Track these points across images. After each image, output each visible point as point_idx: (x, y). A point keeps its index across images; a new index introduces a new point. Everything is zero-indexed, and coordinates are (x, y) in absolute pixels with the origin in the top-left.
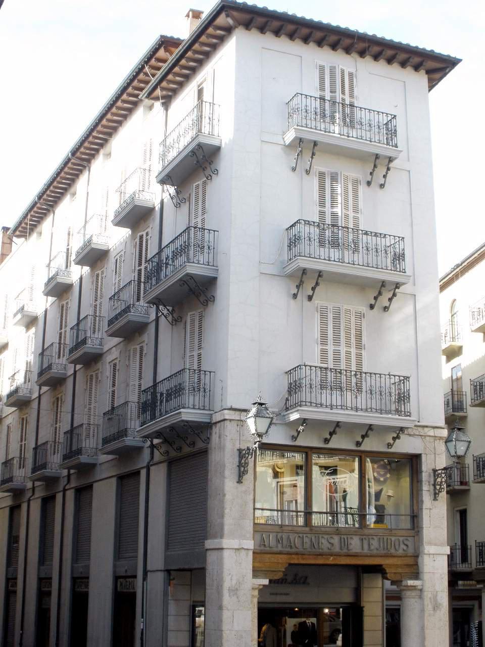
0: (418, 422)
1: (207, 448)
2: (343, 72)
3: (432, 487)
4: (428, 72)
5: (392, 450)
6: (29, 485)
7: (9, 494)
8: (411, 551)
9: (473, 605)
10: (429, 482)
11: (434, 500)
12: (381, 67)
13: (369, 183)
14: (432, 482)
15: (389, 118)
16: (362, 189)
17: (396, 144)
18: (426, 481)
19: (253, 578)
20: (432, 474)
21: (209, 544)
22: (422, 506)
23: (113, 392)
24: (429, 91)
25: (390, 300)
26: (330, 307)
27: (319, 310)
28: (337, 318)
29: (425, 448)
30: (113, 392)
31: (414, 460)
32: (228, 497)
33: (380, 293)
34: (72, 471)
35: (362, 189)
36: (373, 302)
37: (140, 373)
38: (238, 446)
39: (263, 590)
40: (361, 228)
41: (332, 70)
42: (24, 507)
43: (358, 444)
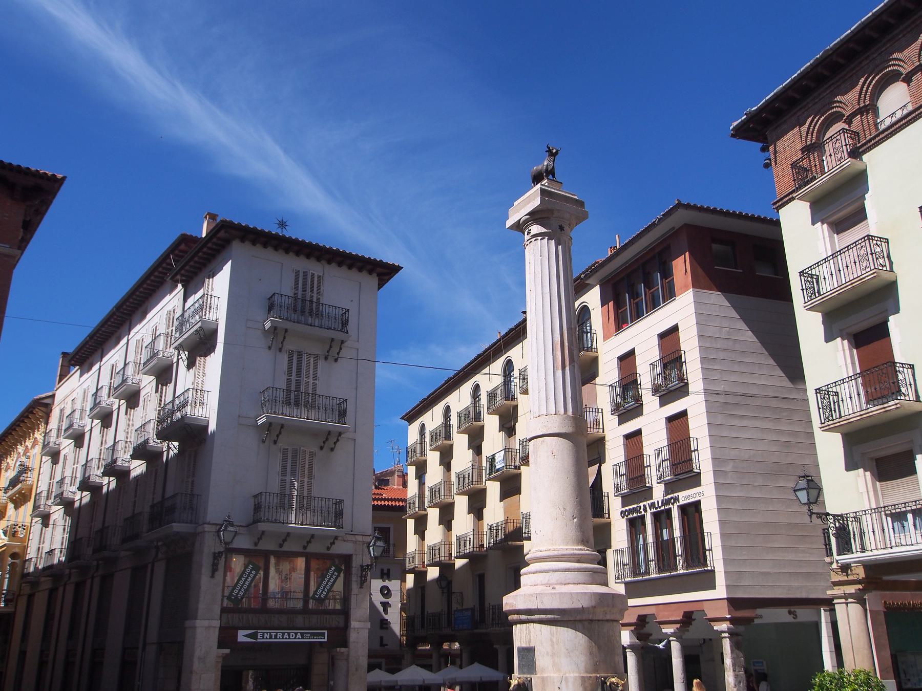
0: (352, 531)
1: (594, 373)
2: (313, 275)
3: (359, 578)
4: (378, 275)
5: (331, 552)
6: (67, 572)
7: (50, 578)
8: (342, 624)
9: (381, 662)
10: (357, 575)
11: (360, 588)
12: (343, 271)
13: (326, 359)
14: (359, 575)
15: (344, 312)
16: (321, 363)
17: (347, 331)
18: (355, 574)
19: (715, 588)
20: (360, 569)
21: (188, 623)
22: (351, 592)
23: (135, 502)
24: (379, 289)
25: (335, 443)
26: (290, 448)
27: (282, 450)
28: (295, 457)
29: (356, 550)
30: (135, 502)
31: (347, 559)
32: (203, 588)
33: (327, 439)
34: (100, 562)
35: (321, 363)
36: (322, 444)
37: (154, 490)
38: (213, 551)
39: (225, 658)
40: (318, 393)
41: (305, 274)
42: (61, 589)
43: (305, 548)
